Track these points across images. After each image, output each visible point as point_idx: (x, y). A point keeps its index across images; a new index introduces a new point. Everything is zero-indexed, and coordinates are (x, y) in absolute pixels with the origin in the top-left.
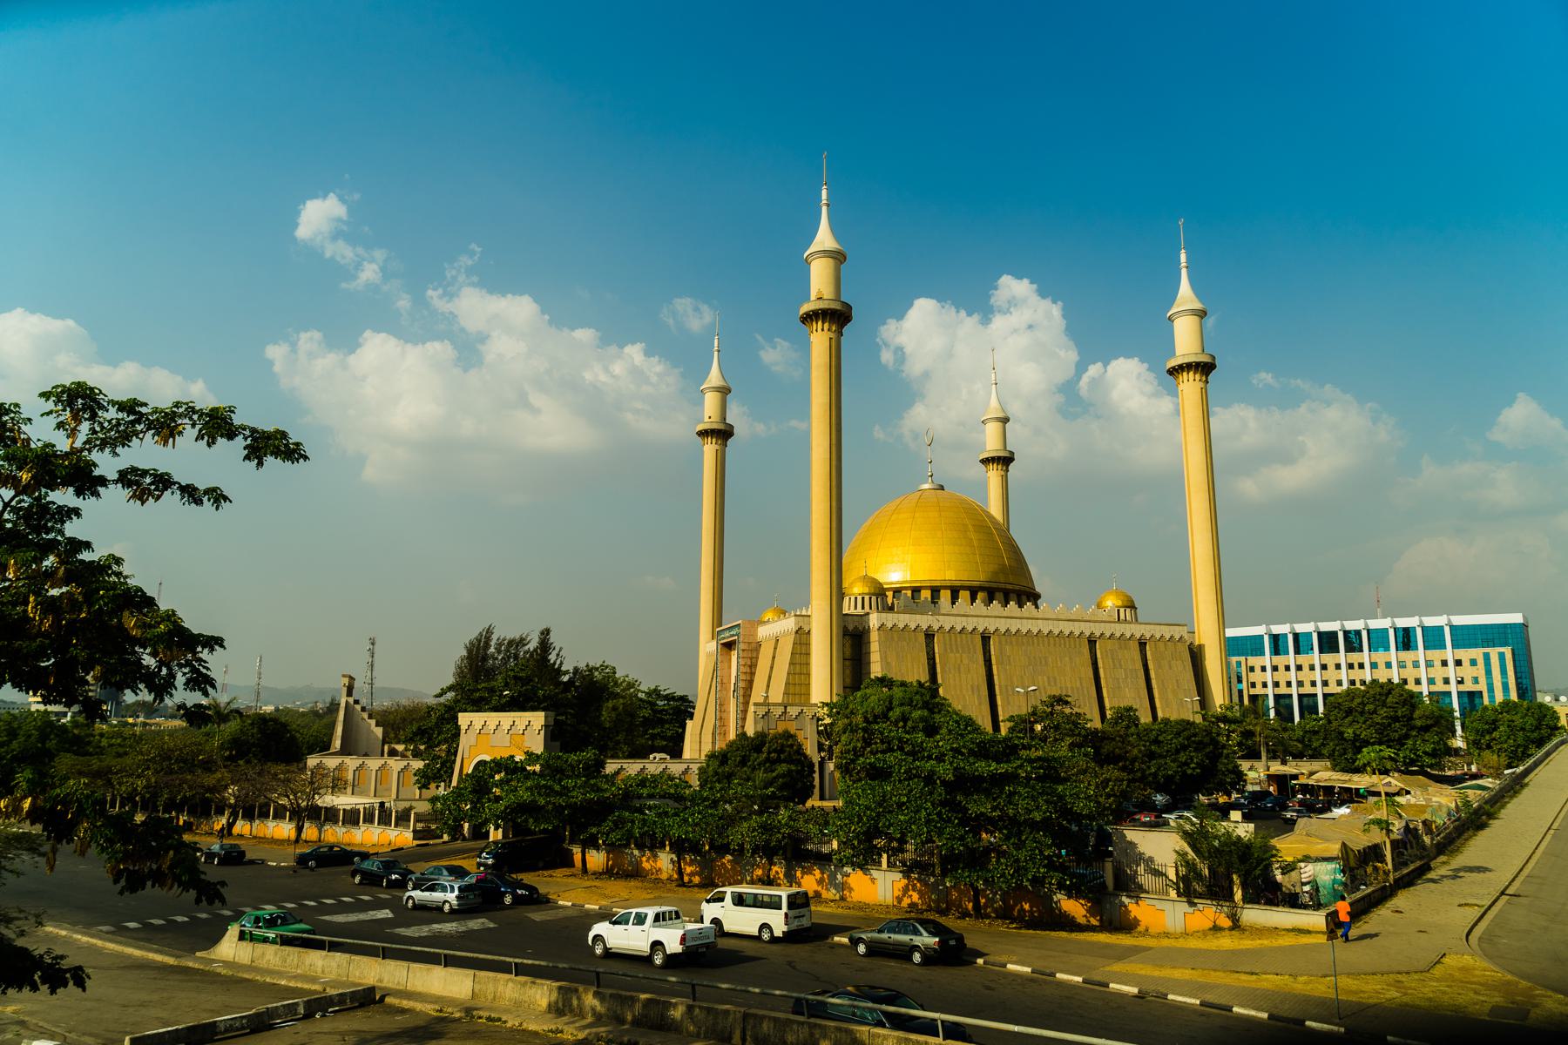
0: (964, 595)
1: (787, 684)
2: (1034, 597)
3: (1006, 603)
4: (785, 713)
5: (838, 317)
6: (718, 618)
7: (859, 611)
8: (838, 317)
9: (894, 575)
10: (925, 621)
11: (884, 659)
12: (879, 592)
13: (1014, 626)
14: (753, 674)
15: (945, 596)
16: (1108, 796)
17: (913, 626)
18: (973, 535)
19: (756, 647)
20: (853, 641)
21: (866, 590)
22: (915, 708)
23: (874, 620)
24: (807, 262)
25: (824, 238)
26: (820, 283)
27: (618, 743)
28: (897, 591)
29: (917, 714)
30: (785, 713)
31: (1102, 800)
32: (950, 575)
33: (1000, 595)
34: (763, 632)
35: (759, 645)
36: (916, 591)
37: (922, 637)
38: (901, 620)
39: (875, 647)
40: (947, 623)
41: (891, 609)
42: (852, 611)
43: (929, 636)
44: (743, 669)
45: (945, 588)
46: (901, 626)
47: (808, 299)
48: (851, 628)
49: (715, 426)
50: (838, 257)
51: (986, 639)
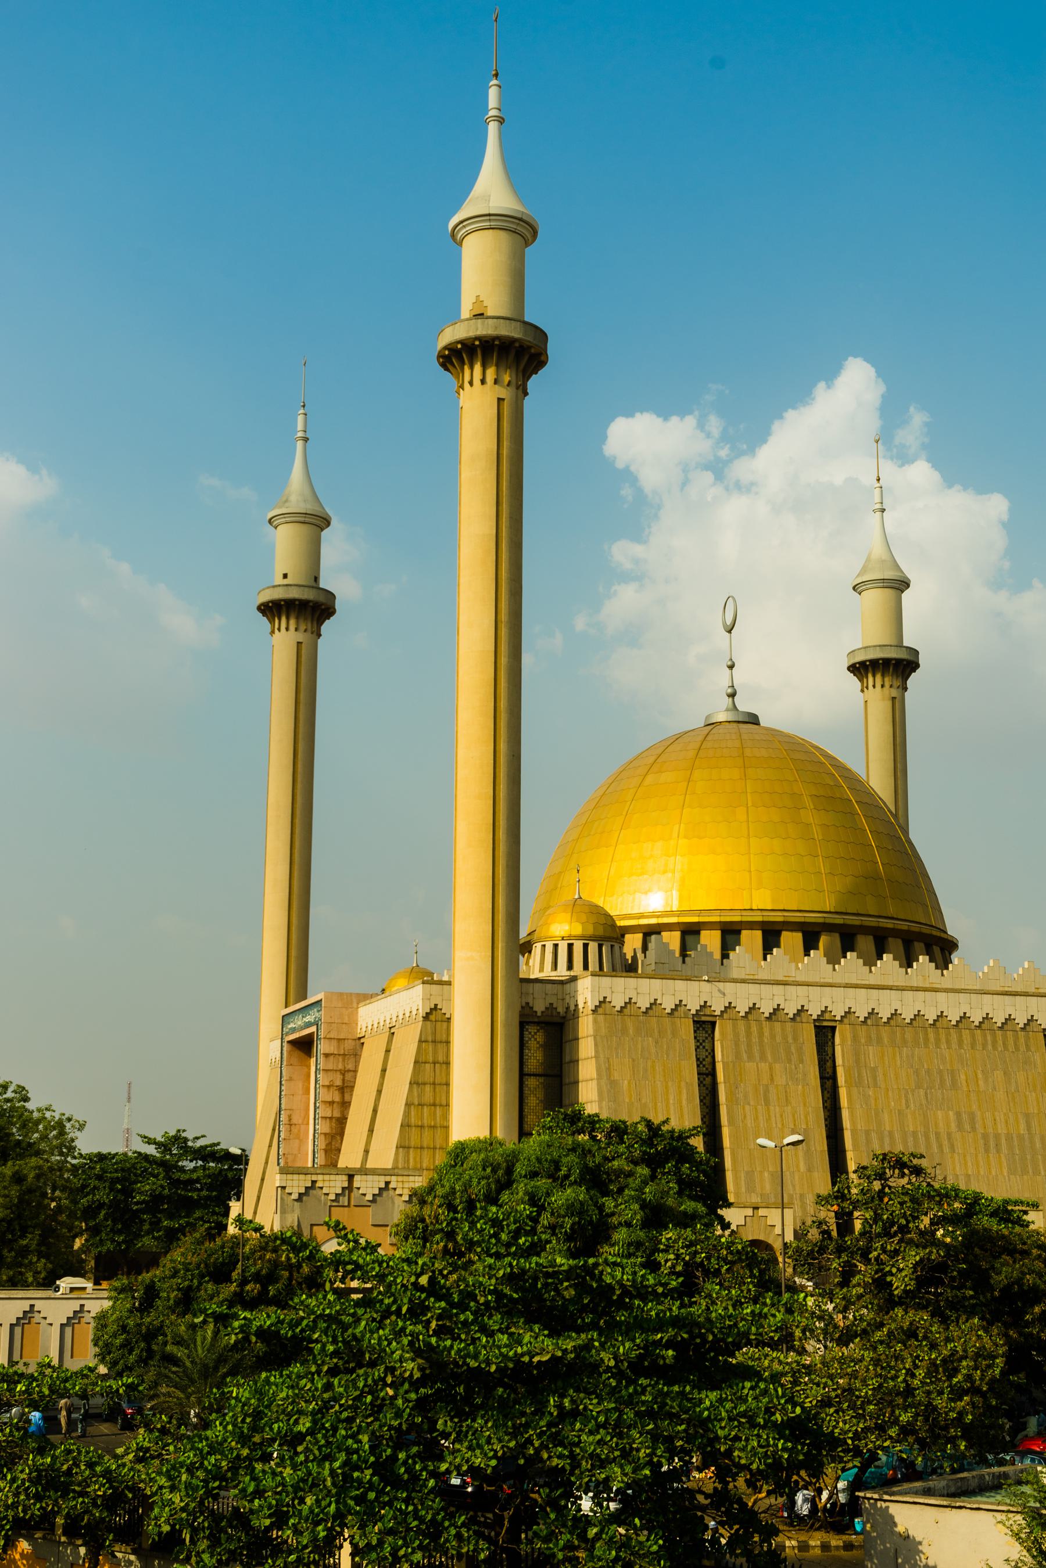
0: (792, 940)
1: (405, 1126)
2: (941, 948)
3: (908, 962)
4: (349, 1189)
5: (515, 354)
6: (297, 982)
7: (562, 972)
8: (515, 354)
9: (650, 891)
10: (693, 994)
11: (605, 1072)
12: (608, 935)
13: (886, 1004)
14: (345, 1104)
15: (752, 939)
16: (957, 1394)
17: (668, 1005)
18: (811, 817)
19: (353, 1050)
20: (541, 1036)
21: (578, 929)
22: (562, 1182)
23: (587, 992)
24: (456, 239)
25: (491, 189)
26: (480, 285)
27: (24, 1252)
28: (650, 932)
29: (560, 1198)
30: (349, 1189)
31: (939, 1402)
32: (762, 898)
33: (866, 942)
34: (370, 1017)
35: (360, 1042)
36: (690, 932)
37: (686, 1030)
38: (642, 990)
39: (586, 1048)
40: (742, 998)
41: (630, 968)
42: (548, 973)
43: (704, 1025)
44: (326, 1095)
45: (751, 925)
46: (644, 1003)
47: (456, 319)
48: (539, 1007)
49: (294, 594)
50: (520, 230)
51: (825, 1033)
